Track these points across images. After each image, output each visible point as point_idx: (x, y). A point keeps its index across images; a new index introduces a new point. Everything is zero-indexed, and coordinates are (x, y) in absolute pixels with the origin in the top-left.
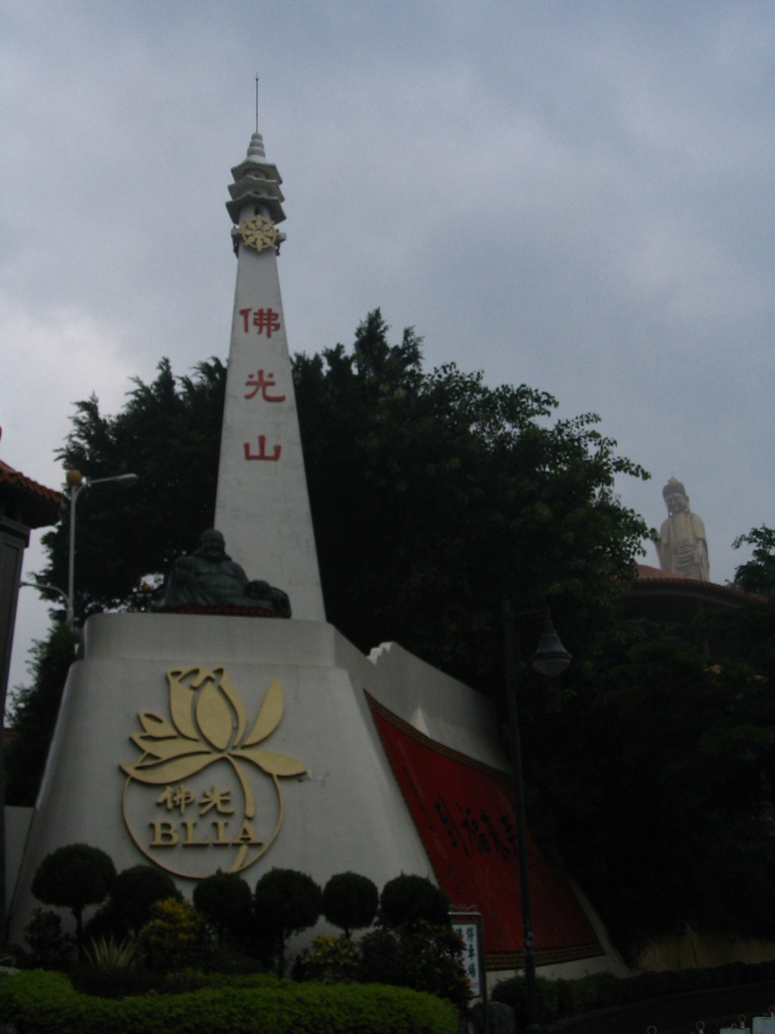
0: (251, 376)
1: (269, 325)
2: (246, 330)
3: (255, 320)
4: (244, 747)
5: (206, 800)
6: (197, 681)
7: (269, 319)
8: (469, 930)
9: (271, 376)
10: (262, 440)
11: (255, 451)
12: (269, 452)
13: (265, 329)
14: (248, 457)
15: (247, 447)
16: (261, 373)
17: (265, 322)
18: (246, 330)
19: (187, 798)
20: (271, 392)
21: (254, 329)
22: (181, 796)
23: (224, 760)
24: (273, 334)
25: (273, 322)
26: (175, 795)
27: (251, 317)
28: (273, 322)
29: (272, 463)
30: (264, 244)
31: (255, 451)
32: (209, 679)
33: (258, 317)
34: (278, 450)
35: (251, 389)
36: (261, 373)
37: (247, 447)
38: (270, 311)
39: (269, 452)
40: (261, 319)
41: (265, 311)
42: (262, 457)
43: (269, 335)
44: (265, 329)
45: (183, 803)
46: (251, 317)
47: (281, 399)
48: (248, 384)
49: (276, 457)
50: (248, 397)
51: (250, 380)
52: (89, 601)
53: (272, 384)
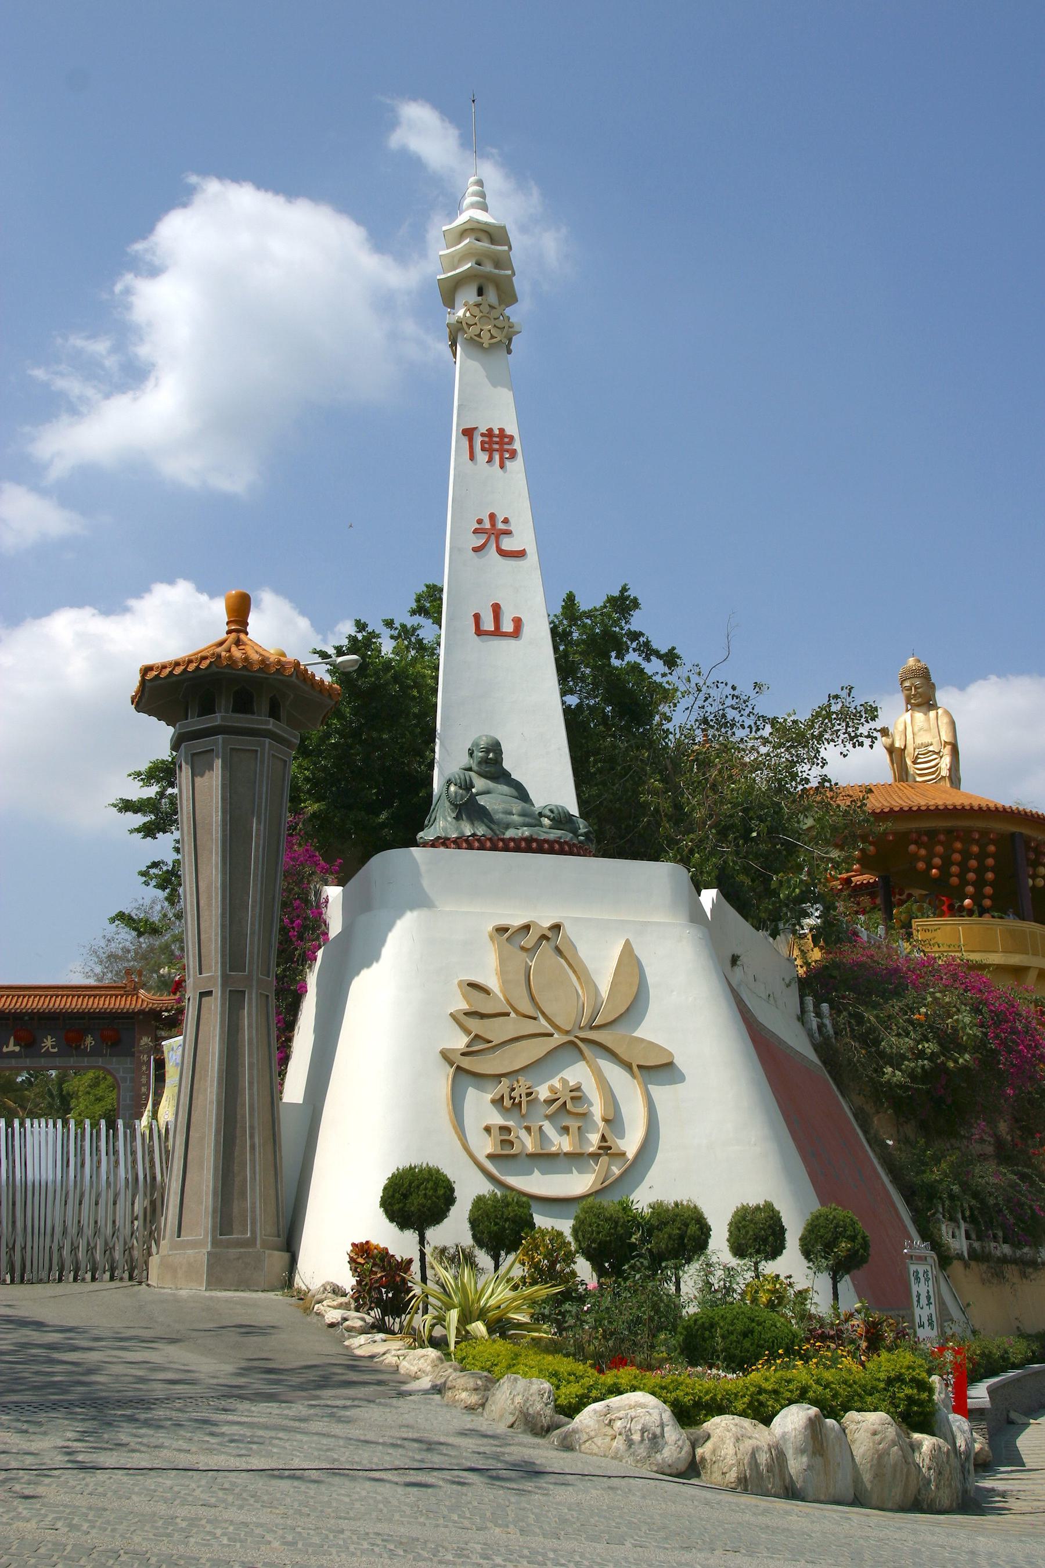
0: (480, 521)
1: (501, 451)
2: (472, 457)
3: (482, 442)
4: (592, 1028)
5: (556, 1096)
6: (529, 941)
7: (501, 443)
8: (926, 1272)
9: (506, 521)
10: (497, 609)
11: (488, 625)
12: (508, 626)
13: (497, 457)
14: (479, 632)
15: (477, 617)
16: (492, 517)
17: (496, 446)
18: (472, 457)
19: (529, 1094)
20: (507, 544)
21: (482, 457)
22: (520, 1090)
23: (571, 1042)
24: (508, 463)
25: (506, 447)
26: (513, 1089)
27: (478, 440)
28: (506, 447)
29: (512, 643)
30: (492, 337)
31: (488, 625)
32: (544, 937)
33: (486, 439)
34: (518, 622)
35: (480, 541)
36: (492, 517)
37: (477, 617)
38: (502, 430)
39: (508, 626)
40: (491, 443)
41: (497, 432)
42: (497, 632)
43: (502, 466)
44: (497, 457)
45: (524, 1099)
46: (478, 440)
47: (521, 554)
48: (476, 531)
49: (516, 633)
50: (476, 550)
51: (478, 526)
52: (383, 825)
53: (508, 533)
